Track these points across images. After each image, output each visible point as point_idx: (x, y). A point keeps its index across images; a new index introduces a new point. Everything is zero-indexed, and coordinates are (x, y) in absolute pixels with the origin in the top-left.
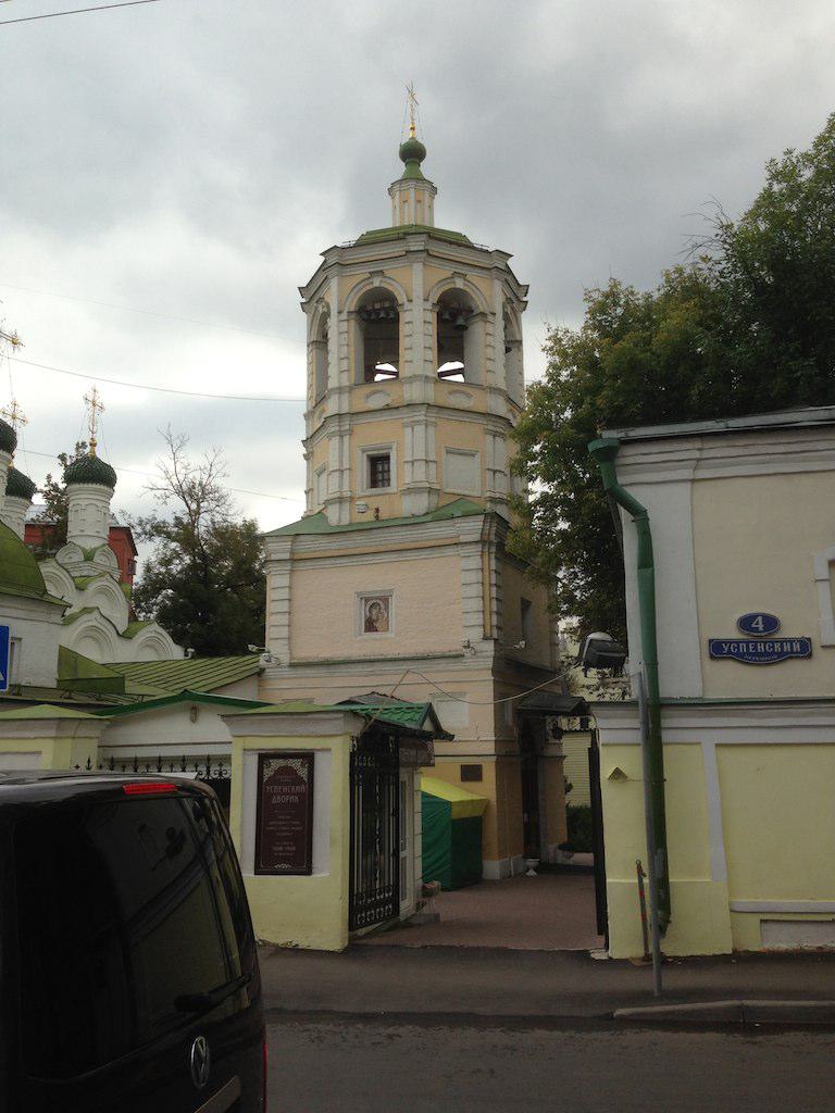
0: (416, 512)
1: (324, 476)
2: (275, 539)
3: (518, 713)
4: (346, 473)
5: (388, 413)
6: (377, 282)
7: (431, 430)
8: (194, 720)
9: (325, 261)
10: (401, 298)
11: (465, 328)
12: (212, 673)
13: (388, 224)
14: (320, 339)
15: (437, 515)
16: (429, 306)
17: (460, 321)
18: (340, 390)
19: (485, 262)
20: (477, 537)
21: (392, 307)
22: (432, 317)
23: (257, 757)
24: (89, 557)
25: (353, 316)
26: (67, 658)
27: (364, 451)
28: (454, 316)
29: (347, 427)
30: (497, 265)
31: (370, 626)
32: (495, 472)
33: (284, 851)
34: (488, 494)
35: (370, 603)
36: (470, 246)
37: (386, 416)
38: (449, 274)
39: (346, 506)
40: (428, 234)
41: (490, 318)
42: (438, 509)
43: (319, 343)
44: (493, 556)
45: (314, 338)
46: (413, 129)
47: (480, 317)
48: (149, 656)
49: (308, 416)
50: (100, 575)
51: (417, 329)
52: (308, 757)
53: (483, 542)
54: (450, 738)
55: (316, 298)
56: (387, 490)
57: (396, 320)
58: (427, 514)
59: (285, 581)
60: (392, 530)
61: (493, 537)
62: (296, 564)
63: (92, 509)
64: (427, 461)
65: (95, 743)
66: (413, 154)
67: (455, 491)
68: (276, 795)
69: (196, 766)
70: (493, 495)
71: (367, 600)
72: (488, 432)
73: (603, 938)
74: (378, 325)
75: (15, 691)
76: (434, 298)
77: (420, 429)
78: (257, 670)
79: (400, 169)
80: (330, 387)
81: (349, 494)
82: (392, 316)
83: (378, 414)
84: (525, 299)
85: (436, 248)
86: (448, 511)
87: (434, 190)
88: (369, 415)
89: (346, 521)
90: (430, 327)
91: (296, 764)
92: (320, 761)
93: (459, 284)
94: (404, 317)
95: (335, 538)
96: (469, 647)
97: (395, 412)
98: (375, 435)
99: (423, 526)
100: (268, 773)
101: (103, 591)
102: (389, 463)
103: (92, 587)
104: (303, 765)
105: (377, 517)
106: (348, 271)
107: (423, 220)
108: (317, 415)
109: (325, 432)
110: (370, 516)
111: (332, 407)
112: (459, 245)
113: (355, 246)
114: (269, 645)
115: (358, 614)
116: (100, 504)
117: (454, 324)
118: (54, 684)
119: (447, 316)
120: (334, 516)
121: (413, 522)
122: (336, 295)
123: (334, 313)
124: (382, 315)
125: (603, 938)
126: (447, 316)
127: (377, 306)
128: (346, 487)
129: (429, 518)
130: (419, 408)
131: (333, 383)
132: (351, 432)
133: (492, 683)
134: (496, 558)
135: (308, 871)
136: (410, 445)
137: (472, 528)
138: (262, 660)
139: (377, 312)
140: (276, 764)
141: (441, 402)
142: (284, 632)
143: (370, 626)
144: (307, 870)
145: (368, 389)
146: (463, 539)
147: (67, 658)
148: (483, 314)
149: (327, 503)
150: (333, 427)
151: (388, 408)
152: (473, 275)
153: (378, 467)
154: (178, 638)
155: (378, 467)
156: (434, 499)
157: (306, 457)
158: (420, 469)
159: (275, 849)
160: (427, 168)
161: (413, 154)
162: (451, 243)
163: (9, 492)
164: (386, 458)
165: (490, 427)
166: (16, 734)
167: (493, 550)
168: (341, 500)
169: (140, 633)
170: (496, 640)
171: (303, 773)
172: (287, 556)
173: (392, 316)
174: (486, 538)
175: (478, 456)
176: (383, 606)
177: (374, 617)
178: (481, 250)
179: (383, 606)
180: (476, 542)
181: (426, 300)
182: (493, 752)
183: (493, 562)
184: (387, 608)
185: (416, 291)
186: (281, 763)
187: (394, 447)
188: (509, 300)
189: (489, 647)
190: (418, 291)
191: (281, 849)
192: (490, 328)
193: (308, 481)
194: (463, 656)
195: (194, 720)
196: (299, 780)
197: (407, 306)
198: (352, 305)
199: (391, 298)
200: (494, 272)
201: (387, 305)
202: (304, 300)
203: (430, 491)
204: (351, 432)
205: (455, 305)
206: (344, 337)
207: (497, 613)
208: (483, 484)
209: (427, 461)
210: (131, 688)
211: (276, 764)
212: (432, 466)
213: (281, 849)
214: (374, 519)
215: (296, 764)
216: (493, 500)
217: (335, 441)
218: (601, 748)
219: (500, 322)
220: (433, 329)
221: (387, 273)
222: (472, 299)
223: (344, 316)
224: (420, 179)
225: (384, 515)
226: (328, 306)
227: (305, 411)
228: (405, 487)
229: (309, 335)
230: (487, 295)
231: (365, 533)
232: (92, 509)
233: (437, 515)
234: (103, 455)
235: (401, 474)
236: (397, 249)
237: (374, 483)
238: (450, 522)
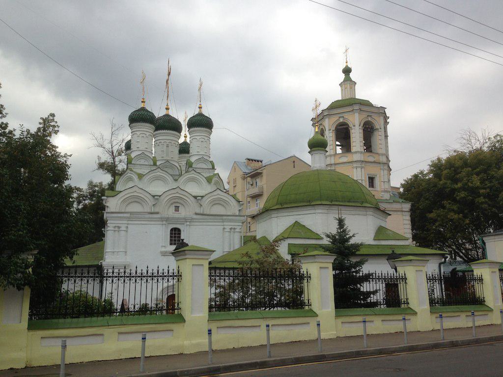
10: (351, 125)
19: (376, 111)
22: (361, 131)
32: (384, 182)
37: (373, 165)
41: (380, 130)
46: (347, 62)
55: (138, 149)
79: (343, 76)
87: (356, 83)
93: (370, 119)
94: (352, 131)
107: (345, 97)
116: (206, 138)
122: (329, 125)
123: (327, 129)
151: (374, 162)
156: (366, 184)
160: (352, 75)
166: (297, 213)
185: (355, 123)
187: (378, 176)
190: (357, 123)
192: (380, 133)
199: (347, 124)
200: (380, 114)
220: (362, 135)
224: (351, 80)
230: (378, 122)
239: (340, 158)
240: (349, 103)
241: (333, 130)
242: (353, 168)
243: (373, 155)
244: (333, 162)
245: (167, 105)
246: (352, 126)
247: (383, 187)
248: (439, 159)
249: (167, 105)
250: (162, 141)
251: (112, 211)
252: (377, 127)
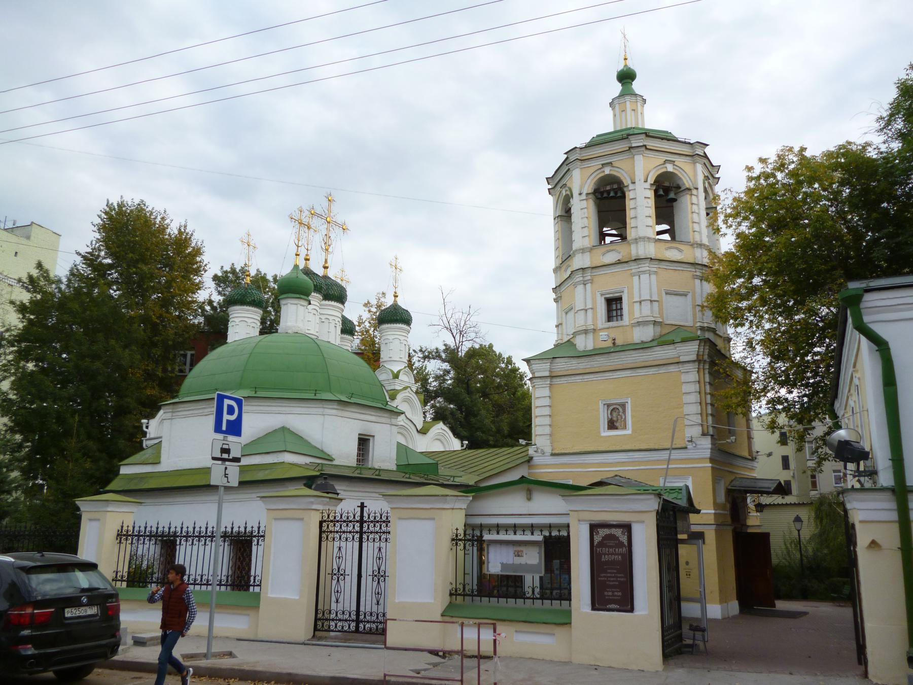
0: (644, 340)
1: (571, 314)
2: (537, 362)
3: (729, 492)
4: (590, 312)
5: (620, 266)
6: (607, 171)
7: (653, 277)
8: (529, 499)
9: (567, 158)
10: (626, 181)
11: (675, 200)
12: (492, 459)
13: (611, 129)
14: (564, 214)
15: (661, 341)
16: (647, 185)
17: (672, 195)
18: (583, 250)
20: (694, 357)
21: (613, 190)
23: (588, 526)
24: (396, 376)
25: (590, 196)
26: (402, 449)
27: (602, 295)
28: (667, 190)
29: (589, 278)
30: (696, 152)
31: (612, 425)
33: (613, 595)
34: (698, 324)
35: (611, 408)
36: (676, 140)
38: (662, 162)
39: (591, 336)
40: (646, 133)
41: (694, 192)
42: (661, 336)
43: (565, 215)
44: (707, 371)
45: (558, 213)
47: (687, 192)
48: (437, 447)
49: (556, 270)
50: (405, 388)
51: (641, 204)
52: (627, 528)
53: (699, 360)
54: (698, 512)
55: (560, 185)
56: (620, 323)
57: (623, 197)
58: (653, 340)
59: (547, 392)
60: (627, 353)
61: (706, 357)
62: (554, 380)
63: (397, 342)
64: (651, 301)
65: (463, 513)
66: (626, 77)
67: (673, 323)
68: (605, 554)
69: (541, 531)
70: (702, 325)
71: (609, 405)
72: (695, 277)
73: (863, 667)
74: (610, 201)
75: (377, 473)
76: (651, 180)
77: (644, 277)
78: (527, 458)
79: (618, 87)
80: (574, 248)
81: (592, 327)
82: (619, 194)
83: (612, 267)
84: (717, 176)
85: (651, 143)
86: (670, 338)
87: (644, 101)
88: (604, 268)
89: (590, 347)
90: (649, 201)
91: (618, 532)
92: (637, 530)
93: (670, 168)
94: (629, 195)
95: (583, 360)
96: (691, 441)
97: (625, 265)
98: (610, 283)
99: (649, 350)
100: (597, 539)
101: (407, 400)
102: (621, 303)
103: (400, 397)
104: (623, 533)
105: (614, 343)
106: (586, 164)
107: (637, 122)
108: (563, 269)
109: (570, 282)
110: (609, 344)
111: (579, 261)
112: (668, 140)
113: (586, 147)
114: (535, 439)
115: (603, 417)
116: (402, 338)
117: (667, 194)
118: (394, 468)
119: (661, 192)
120: (584, 343)
121: (643, 347)
122: (582, 182)
123: (575, 193)
124: (612, 194)
125: (863, 667)
126: (661, 192)
127: (608, 188)
128: (590, 322)
129: (654, 343)
130: (644, 261)
131: (575, 246)
132: (592, 281)
133: (710, 472)
134: (709, 373)
135: (631, 610)
136: (642, 292)
137: (690, 350)
138: (531, 451)
139: (608, 192)
140: (603, 532)
141: (660, 257)
142: (547, 430)
143: (612, 425)
144: (631, 610)
145: (603, 249)
146: (682, 359)
147: (402, 449)
148: (689, 189)
149: (575, 334)
150: (578, 278)
151: (619, 262)
152: (679, 161)
153: (614, 305)
154: (456, 435)
155: (614, 305)
156: (658, 329)
157: (556, 300)
158: (646, 307)
159: (606, 593)
160: (636, 86)
161: (626, 77)
162: (662, 139)
163: (343, 331)
164: (619, 300)
165: (698, 274)
167: (707, 366)
168: (586, 332)
169: (431, 430)
170: (712, 436)
171: (624, 539)
172: (547, 374)
173: (619, 194)
174: (701, 358)
175: (689, 296)
176: (621, 410)
177: (615, 419)
178: (685, 143)
179: (621, 410)
180: (694, 361)
181: (646, 181)
182: (713, 522)
183: (707, 376)
184: (624, 412)
185: (639, 177)
186: (607, 531)
187: (626, 291)
188: (706, 178)
189: (707, 443)
191: (610, 594)
192: (694, 200)
193: (558, 318)
194: (686, 448)
195: (529, 499)
196: (621, 545)
197: (631, 187)
198: (589, 187)
201: (615, 186)
202: (550, 187)
203: (655, 323)
204: (592, 281)
205: (667, 184)
206: (584, 213)
207: (712, 415)
208: (694, 315)
209: (651, 301)
210: (442, 471)
211: (603, 532)
212: (656, 305)
213: (610, 594)
214: (612, 345)
215: (618, 532)
216: (702, 329)
217: (580, 288)
218: (858, 527)
219: (702, 195)
220: (629, 204)
221: (614, 164)
222: (680, 178)
223: (584, 197)
225: (618, 342)
226: (570, 190)
227: (554, 267)
228: (636, 321)
229: (555, 211)
230: (691, 174)
231: (606, 356)
232: (397, 342)
233: (661, 341)
234: (403, 303)
235: (630, 311)
236: (622, 146)
237: (610, 318)
238: (672, 347)
239: (604, 254)
240: (628, 139)
241: (587, 194)
242: (633, 275)
243: (682, 247)
244: (587, 264)
245: (326, 261)
246: (629, 182)
247: (637, 314)
248: (121, 205)
249: (326, 261)
250: (331, 318)
251: (152, 436)
252: (687, 183)
